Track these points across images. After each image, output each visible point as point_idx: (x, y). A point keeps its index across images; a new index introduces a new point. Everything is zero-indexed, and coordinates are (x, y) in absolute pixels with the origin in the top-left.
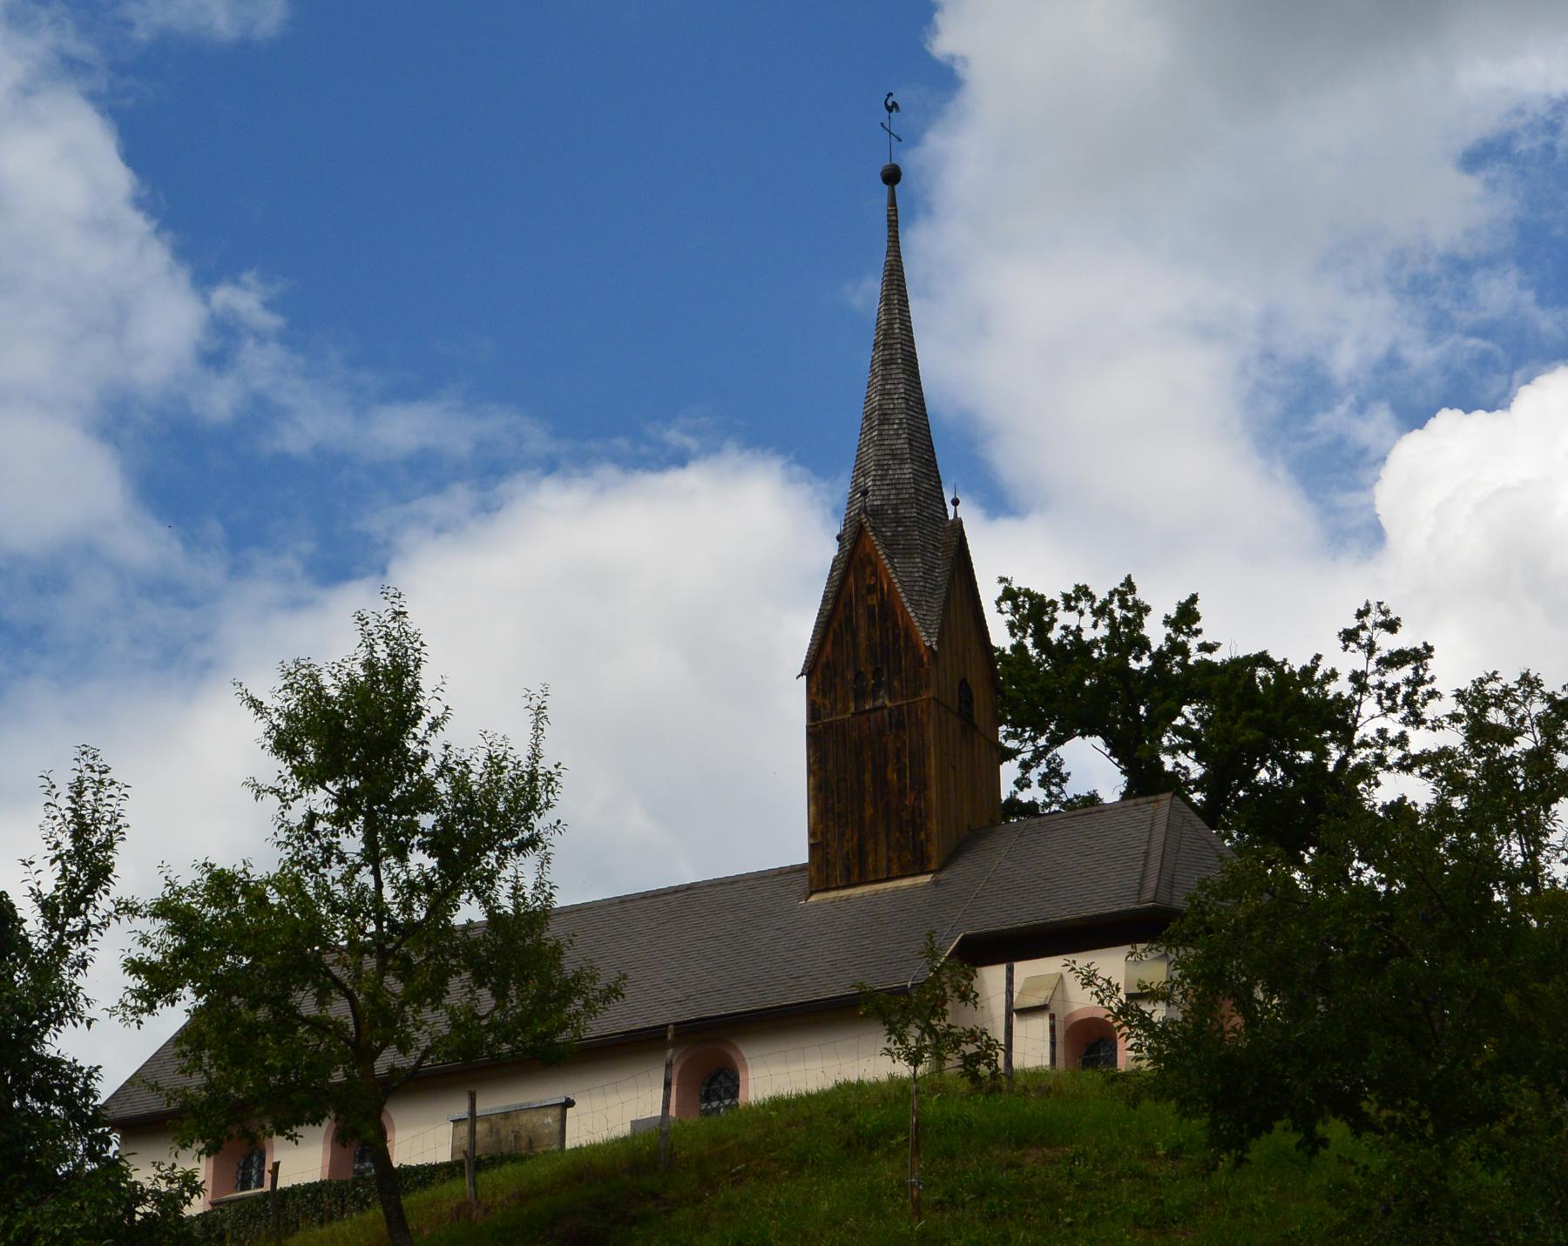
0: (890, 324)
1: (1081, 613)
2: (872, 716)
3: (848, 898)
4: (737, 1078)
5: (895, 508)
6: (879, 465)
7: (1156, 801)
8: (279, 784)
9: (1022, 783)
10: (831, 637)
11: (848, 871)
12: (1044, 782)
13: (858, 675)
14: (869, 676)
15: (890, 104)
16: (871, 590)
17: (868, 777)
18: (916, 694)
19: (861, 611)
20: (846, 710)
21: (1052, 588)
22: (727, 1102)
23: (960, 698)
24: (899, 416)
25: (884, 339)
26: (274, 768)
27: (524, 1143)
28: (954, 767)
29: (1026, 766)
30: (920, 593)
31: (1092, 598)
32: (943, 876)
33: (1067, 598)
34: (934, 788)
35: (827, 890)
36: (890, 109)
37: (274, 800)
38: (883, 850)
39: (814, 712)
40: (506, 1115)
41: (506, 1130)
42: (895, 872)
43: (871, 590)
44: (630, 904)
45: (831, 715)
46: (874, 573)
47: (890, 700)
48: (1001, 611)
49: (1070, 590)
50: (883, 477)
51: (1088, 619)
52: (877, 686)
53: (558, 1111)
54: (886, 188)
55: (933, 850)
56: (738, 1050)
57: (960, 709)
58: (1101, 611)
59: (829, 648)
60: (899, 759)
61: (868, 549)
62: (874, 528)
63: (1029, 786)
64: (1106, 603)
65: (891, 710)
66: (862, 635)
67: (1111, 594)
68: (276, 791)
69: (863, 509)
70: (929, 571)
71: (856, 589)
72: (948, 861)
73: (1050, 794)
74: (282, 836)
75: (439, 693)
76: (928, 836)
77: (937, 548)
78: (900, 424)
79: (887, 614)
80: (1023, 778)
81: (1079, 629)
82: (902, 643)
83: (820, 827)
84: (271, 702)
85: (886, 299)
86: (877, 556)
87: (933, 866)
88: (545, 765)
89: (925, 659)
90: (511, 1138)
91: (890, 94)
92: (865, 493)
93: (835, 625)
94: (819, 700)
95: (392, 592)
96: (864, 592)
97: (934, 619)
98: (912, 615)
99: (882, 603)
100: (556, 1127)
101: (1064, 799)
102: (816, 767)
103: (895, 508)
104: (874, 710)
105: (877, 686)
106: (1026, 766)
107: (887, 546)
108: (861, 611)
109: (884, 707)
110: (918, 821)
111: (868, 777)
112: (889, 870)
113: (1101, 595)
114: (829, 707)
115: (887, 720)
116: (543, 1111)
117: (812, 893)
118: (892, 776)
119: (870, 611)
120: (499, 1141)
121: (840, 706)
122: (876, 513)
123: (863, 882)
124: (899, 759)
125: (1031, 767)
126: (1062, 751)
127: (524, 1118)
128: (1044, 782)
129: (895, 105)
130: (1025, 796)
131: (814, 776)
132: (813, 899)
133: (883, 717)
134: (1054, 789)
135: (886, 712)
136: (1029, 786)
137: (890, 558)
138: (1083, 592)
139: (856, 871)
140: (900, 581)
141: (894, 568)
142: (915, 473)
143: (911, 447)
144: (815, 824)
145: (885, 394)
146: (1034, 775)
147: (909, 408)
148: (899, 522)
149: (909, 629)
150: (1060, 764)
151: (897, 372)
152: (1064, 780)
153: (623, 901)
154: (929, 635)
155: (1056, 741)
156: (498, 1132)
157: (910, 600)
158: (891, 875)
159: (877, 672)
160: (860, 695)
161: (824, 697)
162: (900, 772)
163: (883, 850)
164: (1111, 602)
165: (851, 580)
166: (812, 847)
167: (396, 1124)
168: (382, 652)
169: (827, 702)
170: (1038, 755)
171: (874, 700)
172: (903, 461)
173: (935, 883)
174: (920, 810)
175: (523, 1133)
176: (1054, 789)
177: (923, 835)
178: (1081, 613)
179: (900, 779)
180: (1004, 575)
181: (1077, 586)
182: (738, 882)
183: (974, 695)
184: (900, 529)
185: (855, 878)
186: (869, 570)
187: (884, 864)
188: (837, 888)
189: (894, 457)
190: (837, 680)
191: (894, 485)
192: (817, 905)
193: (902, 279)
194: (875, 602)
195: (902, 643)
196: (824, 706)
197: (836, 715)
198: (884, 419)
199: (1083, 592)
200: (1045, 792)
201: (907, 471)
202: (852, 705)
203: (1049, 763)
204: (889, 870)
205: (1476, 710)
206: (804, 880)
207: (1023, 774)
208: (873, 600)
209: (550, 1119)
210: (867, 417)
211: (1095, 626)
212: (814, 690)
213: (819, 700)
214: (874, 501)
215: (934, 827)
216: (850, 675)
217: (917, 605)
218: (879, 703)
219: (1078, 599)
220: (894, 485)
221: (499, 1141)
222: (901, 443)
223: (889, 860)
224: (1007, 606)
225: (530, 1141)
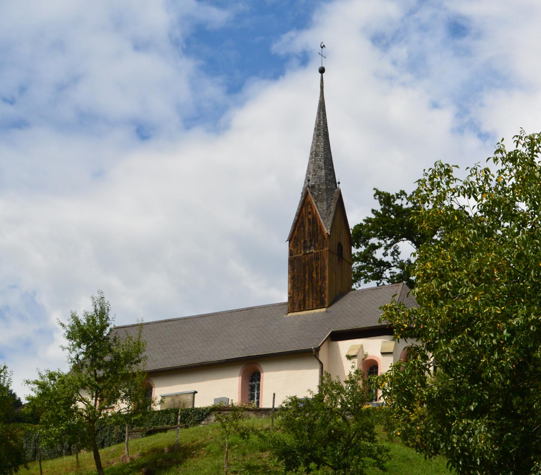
0: (320, 122)
1: (402, 199)
2: (309, 255)
3: (299, 316)
4: (260, 375)
5: (319, 185)
6: (314, 171)
7: (398, 286)
8: (69, 347)
9: (385, 255)
10: (297, 228)
11: (300, 305)
12: (392, 254)
13: (305, 241)
14: (308, 242)
15: (322, 46)
16: (310, 213)
17: (307, 276)
18: (323, 249)
19: (306, 220)
20: (301, 253)
21: (393, 191)
22: (257, 382)
23: (338, 249)
24: (321, 154)
25: (318, 127)
26: (67, 343)
27: (182, 404)
28: (335, 272)
29: (386, 248)
30: (325, 215)
31: (406, 195)
32: (329, 309)
33: (397, 195)
34: (327, 280)
35: (293, 312)
36: (322, 47)
37: (67, 351)
38: (311, 300)
39: (291, 253)
40: (177, 395)
41: (177, 400)
42: (315, 307)
43: (310, 213)
44: (233, 313)
45: (296, 254)
46: (311, 208)
47: (315, 250)
48: (375, 199)
49: (398, 192)
50: (315, 175)
51: (405, 201)
52: (311, 245)
53: (192, 395)
54: (320, 74)
55: (326, 300)
56: (260, 366)
57: (338, 253)
58: (410, 199)
59: (296, 232)
60: (317, 270)
61: (309, 200)
62: (311, 193)
63: (387, 255)
64: (411, 196)
65: (315, 254)
66: (307, 228)
67: (413, 193)
68: (68, 348)
69: (308, 186)
70: (329, 207)
71: (305, 213)
72: (330, 306)
73: (394, 259)
74: (70, 361)
75: (114, 319)
76: (325, 295)
77: (332, 199)
78: (322, 156)
79: (314, 221)
80: (385, 252)
81: (402, 205)
82: (319, 232)
83: (292, 291)
84: (66, 323)
85: (319, 113)
86: (312, 202)
87: (327, 305)
88: (142, 340)
89: (326, 237)
90: (178, 403)
91: (322, 43)
92: (309, 181)
93: (298, 224)
94: (292, 249)
95: (100, 291)
96: (307, 214)
97: (330, 223)
98: (322, 222)
99: (313, 218)
100: (192, 400)
101: (399, 261)
102: (291, 271)
103: (319, 185)
104: (310, 253)
105: (311, 245)
106: (386, 248)
107: (316, 198)
108: (306, 220)
109: (313, 252)
110: (322, 291)
111: (307, 276)
112: (313, 306)
113: (409, 193)
114: (295, 252)
115: (313, 257)
116: (188, 395)
117: (289, 313)
118: (314, 275)
119: (309, 220)
120: (174, 403)
121: (299, 251)
122: (313, 187)
123: (304, 310)
124: (317, 270)
125: (388, 249)
126: (398, 244)
127: (182, 397)
128: (392, 254)
129: (324, 46)
130: (385, 259)
131: (290, 274)
132: (289, 315)
133: (312, 255)
134: (395, 257)
135: (313, 254)
136: (387, 255)
137: (316, 203)
138: (403, 193)
139: (302, 306)
140: (319, 211)
141: (317, 206)
142: (326, 173)
143: (325, 165)
144: (290, 290)
145: (317, 146)
146: (390, 251)
147: (325, 151)
148: (319, 190)
149: (321, 227)
150: (398, 248)
151: (321, 139)
152: (399, 254)
153: (231, 312)
154: (327, 229)
155: (397, 240)
156: (174, 400)
157: (322, 217)
158: (314, 308)
159: (311, 240)
160: (305, 248)
161: (294, 248)
162: (317, 274)
163: (311, 300)
164: (413, 195)
165: (304, 209)
166: (289, 298)
167: (156, 385)
168: (98, 308)
169: (295, 250)
170: (391, 245)
171: (310, 250)
172: (322, 169)
173: (327, 312)
174: (323, 287)
175: (182, 401)
176: (395, 257)
177: (323, 296)
178: (402, 199)
179: (317, 277)
180: (375, 187)
181: (401, 190)
182: (267, 307)
183: (343, 247)
184: (320, 193)
185: (302, 309)
186: (309, 206)
187: (311, 304)
188: (296, 312)
189: (319, 167)
190: (298, 243)
191: (318, 177)
192: (290, 317)
193: (324, 106)
194: (311, 217)
195: (319, 232)
196: (294, 251)
197: (298, 254)
198: (317, 155)
199: (403, 193)
200: (393, 258)
201: (323, 173)
202: (303, 251)
203: (394, 248)
204: (313, 306)
205: (516, 250)
206: (286, 307)
207: (386, 251)
208: (310, 217)
209: (190, 397)
210: (311, 154)
211: (407, 204)
212: (291, 246)
213: (292, 249)
214: (312, 183)
215: (327, 292)
216: (302, 241)
217: (324, 219)
218: (311, 251)
219: (401, 195)
220: (318, 177)
221: (174, 403)
222: (322, 163)
223: (313, 303)
224: (377, 197)
225: (184, 404)
